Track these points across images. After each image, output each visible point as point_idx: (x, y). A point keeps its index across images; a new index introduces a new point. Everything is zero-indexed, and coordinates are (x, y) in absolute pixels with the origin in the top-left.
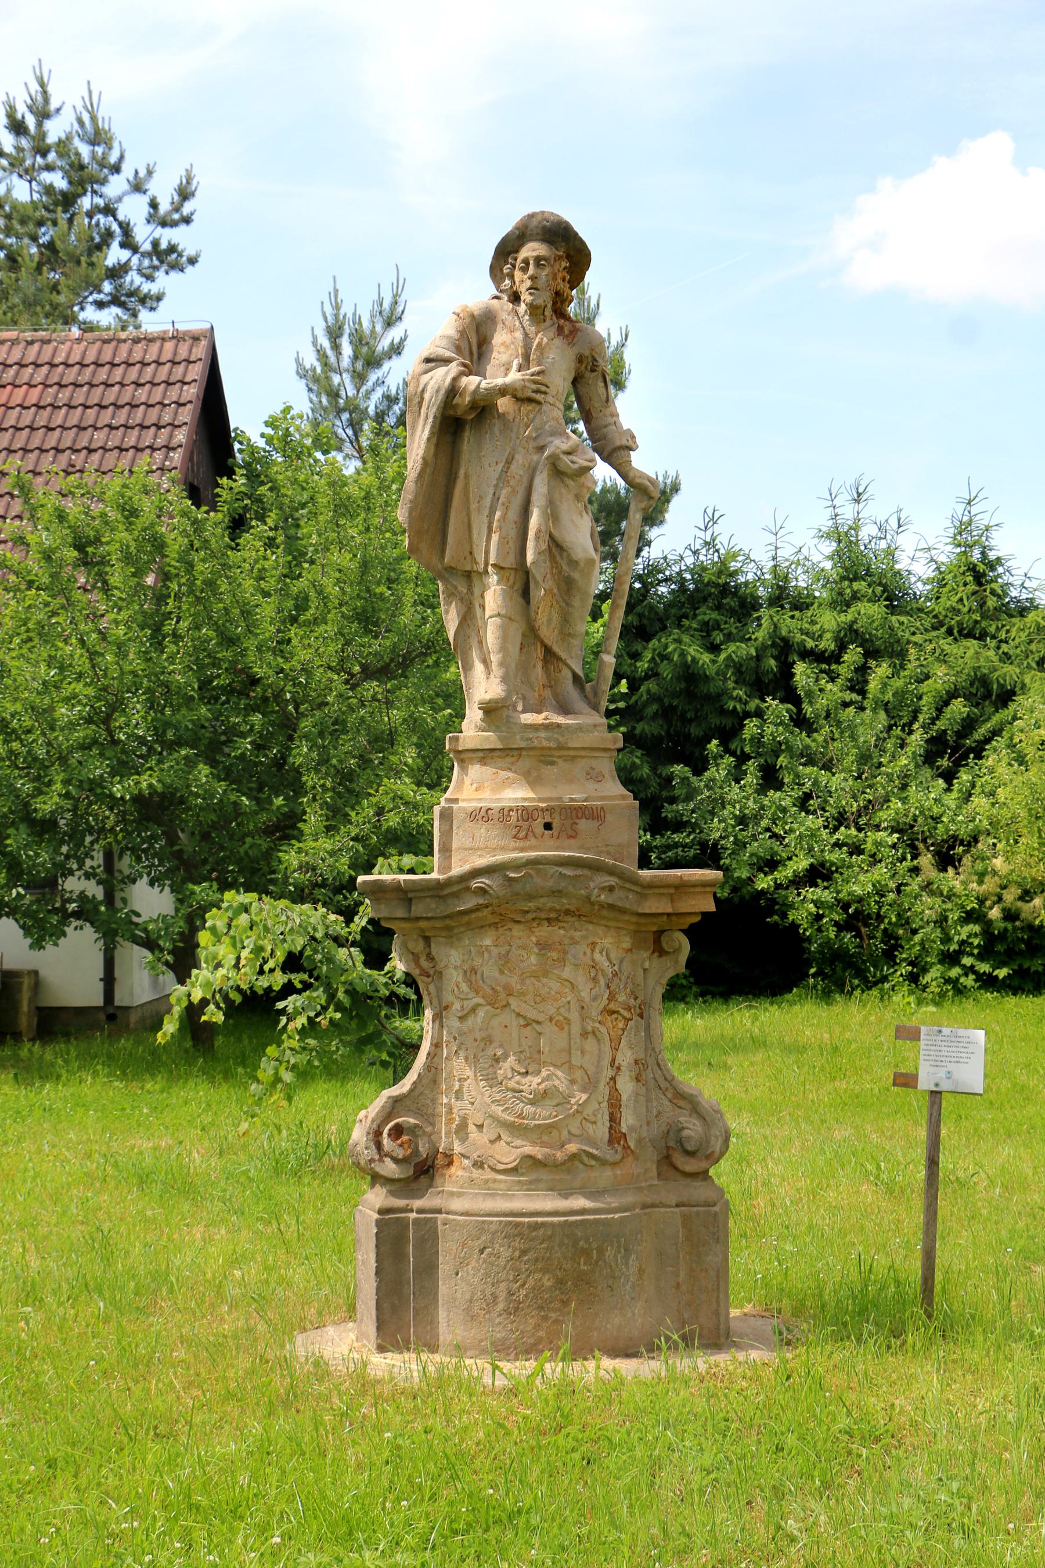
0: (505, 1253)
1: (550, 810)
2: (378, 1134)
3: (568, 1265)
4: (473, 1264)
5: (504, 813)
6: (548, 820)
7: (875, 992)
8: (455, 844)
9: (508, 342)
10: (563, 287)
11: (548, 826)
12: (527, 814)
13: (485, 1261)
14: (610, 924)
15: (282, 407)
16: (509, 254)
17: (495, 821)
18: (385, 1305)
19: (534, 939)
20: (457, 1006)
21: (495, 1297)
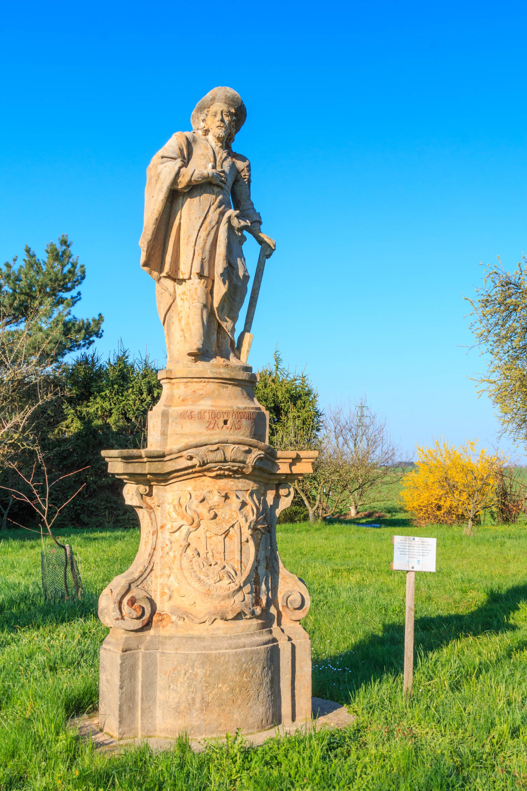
0: (200, 672)
1: (227, 413)
2: (120, 603)
3: (237, 679)
4: (181, 680)
5: (201, 415)
6: (226, 418)
7: (318, 532)
8: (170, 431)
9: (205, 154)
10: (234, 130)
11: (225, 422)
12: (215, 415)
13: (188, 678)
14: (257, 479)
15: (45, 252)
16: (204, 108)
17: (197, 419)
18: (125, 708)
19: (217, 487)
20: (169, 526)
21: (193, 699)
